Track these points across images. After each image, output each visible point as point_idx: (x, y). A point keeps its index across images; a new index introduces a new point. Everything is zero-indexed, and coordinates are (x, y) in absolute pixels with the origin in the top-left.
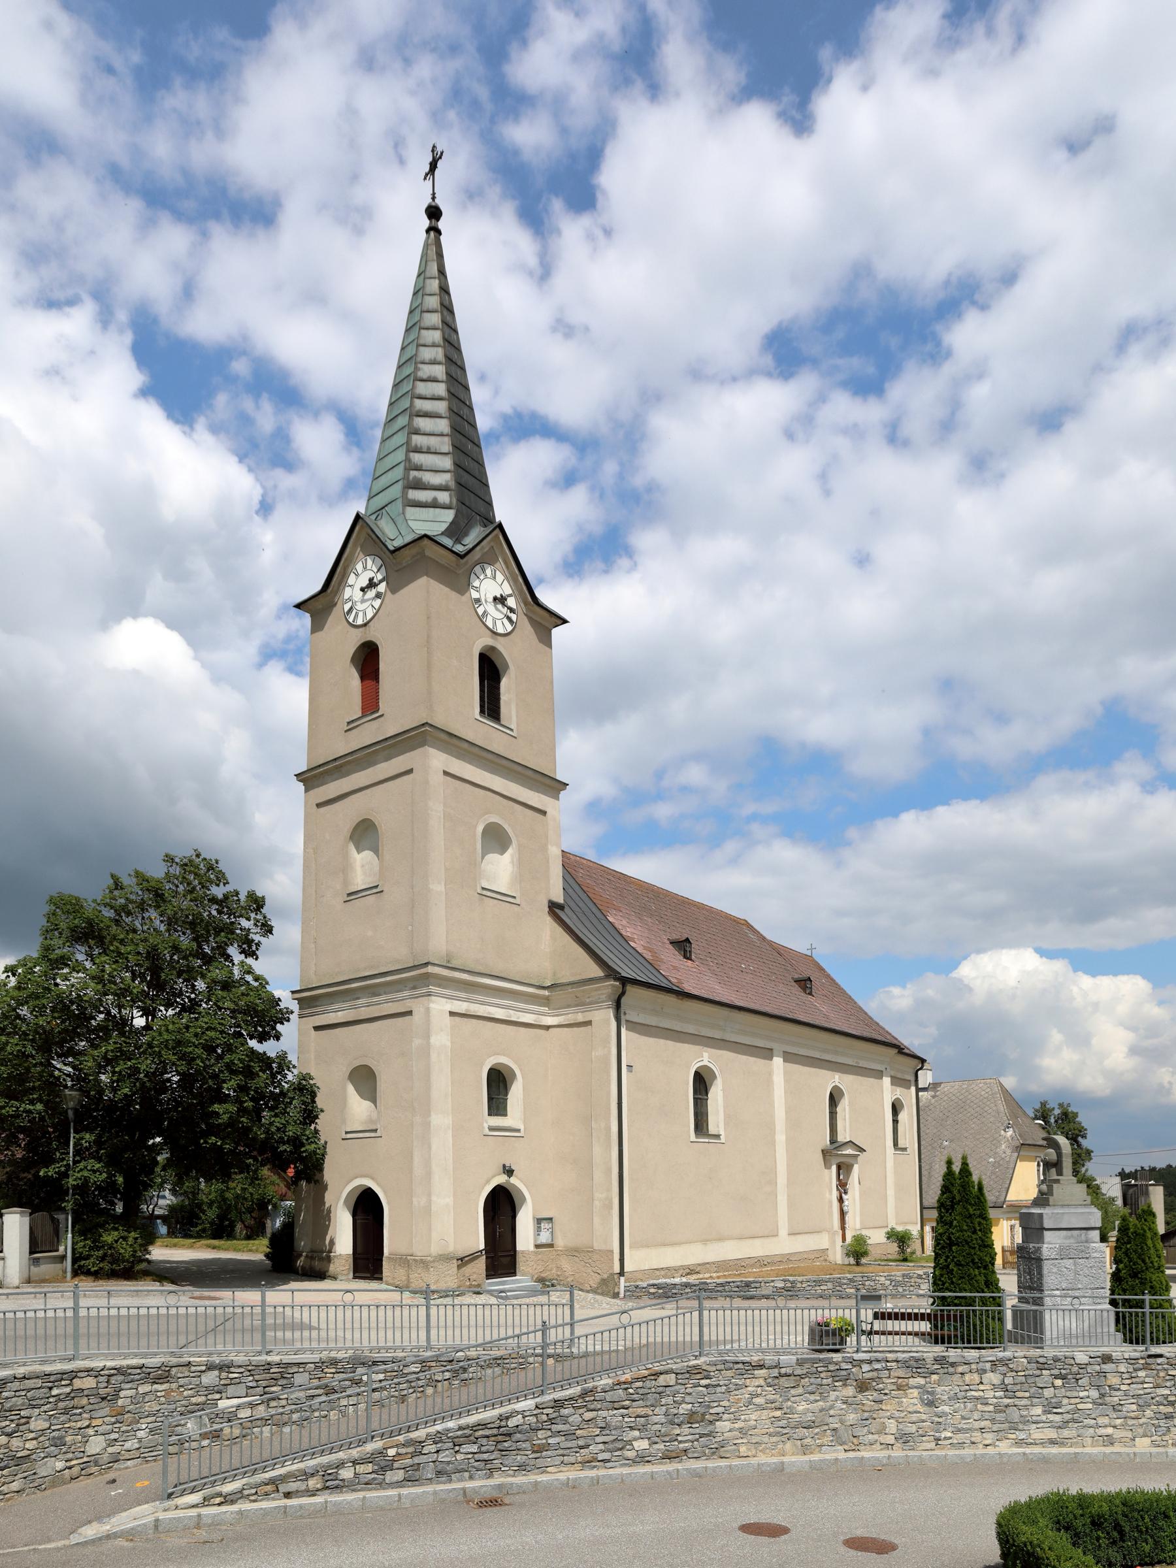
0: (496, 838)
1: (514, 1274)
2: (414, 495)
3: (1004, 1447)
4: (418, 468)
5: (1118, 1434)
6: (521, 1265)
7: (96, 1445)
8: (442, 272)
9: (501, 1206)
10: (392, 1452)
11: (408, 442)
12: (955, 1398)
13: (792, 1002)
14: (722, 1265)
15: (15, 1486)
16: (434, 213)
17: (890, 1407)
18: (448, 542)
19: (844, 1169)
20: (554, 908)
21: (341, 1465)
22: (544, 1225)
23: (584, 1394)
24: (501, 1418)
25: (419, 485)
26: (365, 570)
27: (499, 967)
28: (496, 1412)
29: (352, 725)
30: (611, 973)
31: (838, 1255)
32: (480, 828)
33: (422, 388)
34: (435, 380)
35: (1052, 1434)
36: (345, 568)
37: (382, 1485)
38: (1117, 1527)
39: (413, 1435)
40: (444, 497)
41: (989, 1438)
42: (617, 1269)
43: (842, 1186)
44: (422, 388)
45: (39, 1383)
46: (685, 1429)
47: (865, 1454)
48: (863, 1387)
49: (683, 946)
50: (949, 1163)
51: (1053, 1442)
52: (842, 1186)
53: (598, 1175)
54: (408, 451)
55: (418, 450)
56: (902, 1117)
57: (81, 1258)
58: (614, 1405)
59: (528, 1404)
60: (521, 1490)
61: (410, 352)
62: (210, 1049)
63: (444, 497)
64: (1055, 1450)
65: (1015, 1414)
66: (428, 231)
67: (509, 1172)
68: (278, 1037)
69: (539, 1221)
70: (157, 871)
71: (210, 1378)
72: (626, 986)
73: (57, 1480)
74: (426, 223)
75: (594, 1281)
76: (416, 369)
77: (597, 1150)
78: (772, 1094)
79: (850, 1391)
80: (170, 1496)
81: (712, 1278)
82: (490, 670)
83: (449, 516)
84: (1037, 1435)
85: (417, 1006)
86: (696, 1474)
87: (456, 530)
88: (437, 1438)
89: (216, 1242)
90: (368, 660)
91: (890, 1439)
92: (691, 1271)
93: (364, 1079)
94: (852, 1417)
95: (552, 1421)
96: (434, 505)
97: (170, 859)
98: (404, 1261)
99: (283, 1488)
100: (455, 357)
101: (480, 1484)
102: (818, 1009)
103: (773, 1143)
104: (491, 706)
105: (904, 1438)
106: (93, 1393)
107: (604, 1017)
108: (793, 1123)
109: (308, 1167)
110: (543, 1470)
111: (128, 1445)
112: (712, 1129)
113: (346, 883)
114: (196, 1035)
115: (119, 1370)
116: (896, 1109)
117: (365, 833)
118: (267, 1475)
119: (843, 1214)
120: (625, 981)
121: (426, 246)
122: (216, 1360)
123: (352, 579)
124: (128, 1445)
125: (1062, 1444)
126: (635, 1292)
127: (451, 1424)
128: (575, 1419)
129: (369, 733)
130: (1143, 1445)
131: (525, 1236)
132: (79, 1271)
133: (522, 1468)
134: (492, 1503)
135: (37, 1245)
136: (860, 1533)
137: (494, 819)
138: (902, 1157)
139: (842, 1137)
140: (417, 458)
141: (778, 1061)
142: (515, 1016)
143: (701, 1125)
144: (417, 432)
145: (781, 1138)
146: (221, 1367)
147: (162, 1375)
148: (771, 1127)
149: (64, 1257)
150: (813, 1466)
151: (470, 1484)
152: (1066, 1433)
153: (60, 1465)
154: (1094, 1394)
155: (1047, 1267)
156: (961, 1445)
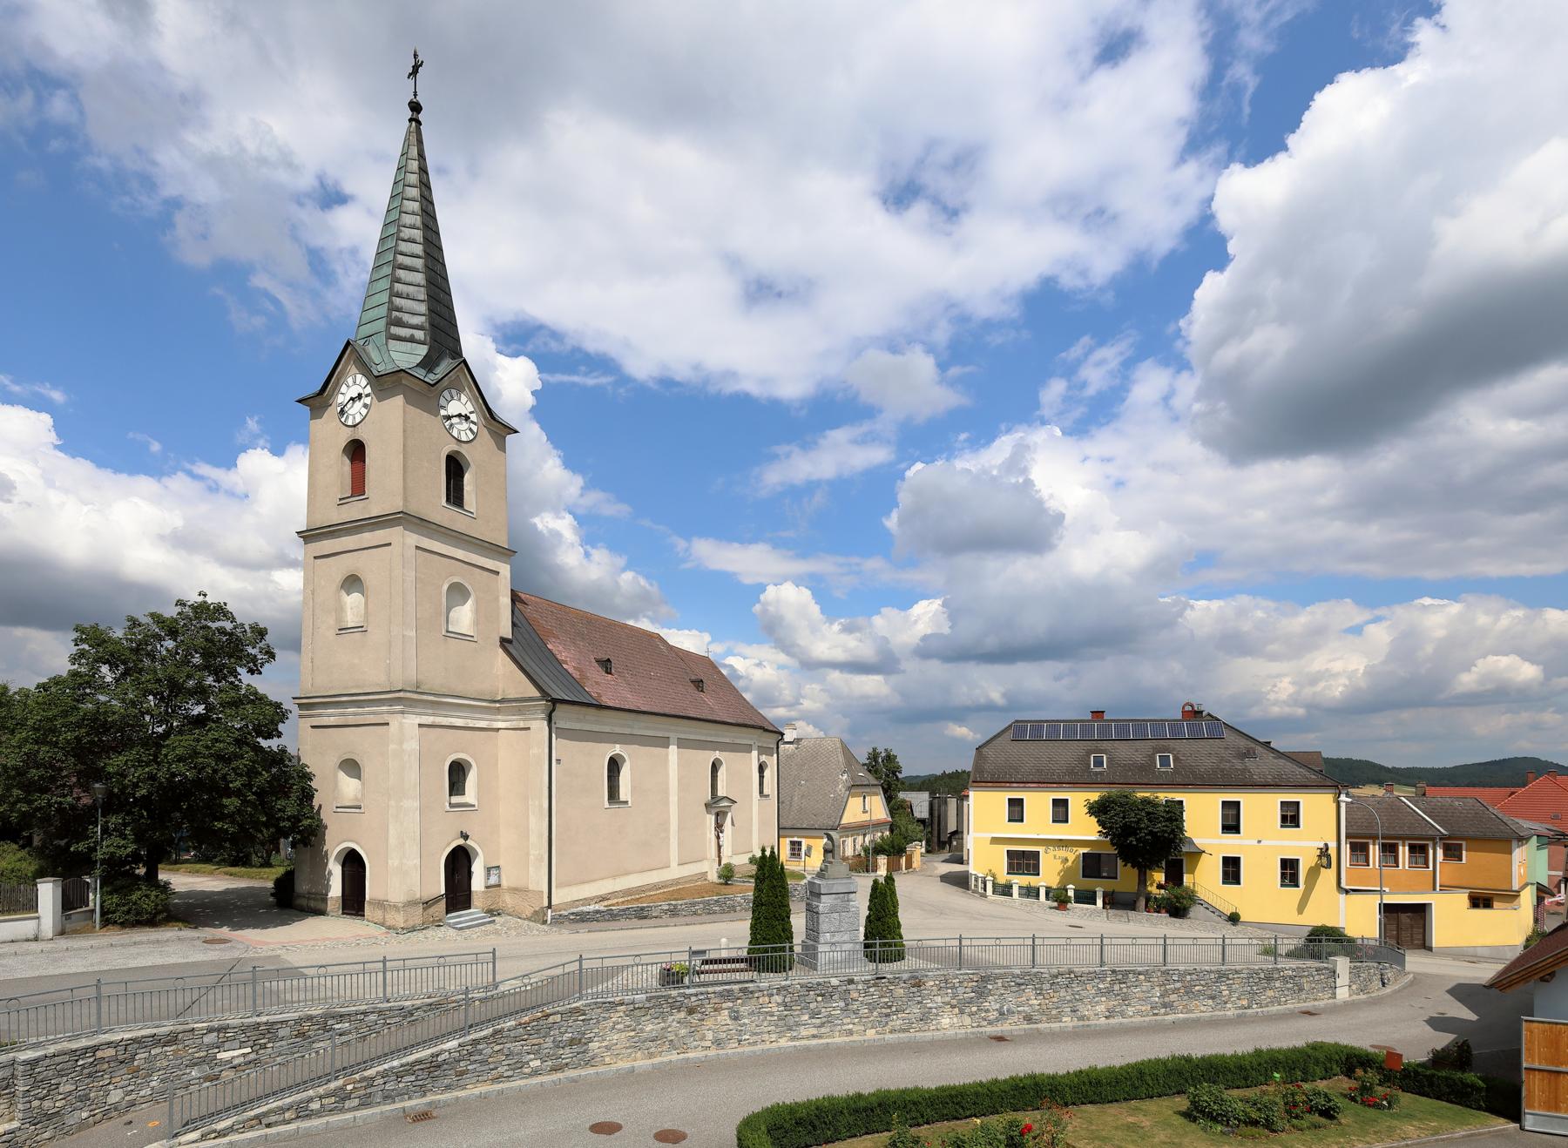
0: (458, 593)
1: (469, 907)
2: (395, 330)
3: (783, 1042)
4: (399, 310)
5: (855, 1028)
6: (476, 901)
7: (115, 1096)
8: (421, 156)
9: (459, 862)
10: (350, 1087)
11: (391, 288)
12: (752, 1013)
13: (687, 701)
14: (628, 892)
15: (46, 1135)
16: (415, 107)
17: (709, 1023)
18: (420, 373)
19: (720, 816)
20: (504, 642)
21: (310, 1100)
22: (493, 872)
23: (495, 1033)
24: (433, 1056)
25: (399, 323)
26: (354, 384)
27: (459, 690)
28: (429, 1052)
29: (343, 501)
30: (545, 694)
31: (713, 876)
32: (445, 587)
33: (403, 247)
34: (414, 242)
35: (814, 1031)
36: (338, 380)
37: (342, 1111)
38: (811, 1123)
39: (366, 1073)
40: (420, 335)
41: (774, 1037)
42: (546, 904)
43: (719, 827)
44: (403, 247)
45: (67, 1058)
46: (567, 1050)
47: (691, 1055)
48: (691, 1011)
49: (606, 665)
50: (763, 850)
51: (814, 1036)
52: (719, 827)
53: (533, 838)
54: (391, 295)
55: (399, 296)
56: (767, 773)
57: (108, 912)
58: (516, 1039)
59: (453, 1044)
60: (446, 1104)
61: (394, 215)
62: (220, 758)
63: (420, 335)
64: (814, 1042)
65: (791, 1021)
66: (411, 120)
67: (466, 837)
68: (279, 735)
69: (489, 870)
70: (171, 612)
71: (210, 1038)
72: (560, 700)
73: (82, 1126)
74: (409, 114)
75: (528, 912)
76: (399, 231)
77: (533, 820)
78: (668, 773)
79: (682, 1015)
80: (176, 1135)
81: (616, 904)
82: (455, 468)
83: (423, 350)
84: (804, 1033)
85: (395, 721)
86: (574, 1080)
87: (428, 363)
88: (384, 1074)
89: (233, 870)
90: (356, 451)
91: (708, 1044)
92: (603, 899)
93: (351, 767)
94: (683, 1032)
95: (470, 1054)
96: (412, 340)
97: (180, 603)
98: (381, 904)
99: (265, 1121)
100: (431, 224)
101: (416, 1103)
102: (709, 703)
103: (667, 803)
104: (455, 495)
105: (718, 1043)
106: (115, 1059)
107: (539, 726)
108: (683, 786)
109: (309, 834)
110: (464, 1087)
111: (142, 1093)
112: (622, 797)
113: (339, 619)
114: (207, 747)
115: (134, 1040)
116: (761, 768)
117: (352, 582)
118: (252, 1113)
119: (719, 847)
120: (555, 702)
121: (409, 132)
122: (215, 1024)
123: (344, 389)
124: (142, 1093)
125: (820, 1037)
126: (559, 920)
127: (395, 1063)
128: (488, 1051)
129: (355, 511)
130: (871, 1033)
131: (478, 883)
132: (107, 921)
133: (448, 1088)
134: (423, 1116)
135: (70, 902)
136: (667, 1126)
137: (456, 580)
138: (765, 801)
139: (720, 794)
140: (398, 301)
141: (673, 749)
142: (471, 723)
143: (613, 794)
144: (399, 281)
145: (674, 799)
146: (219, 1030)
147: (172, 1039)
148: (666, 792)
149: (93, 911)
150: (656, 1068)
151: (408, 1104)
152: (823, 1030)
153: (85, 1115)
154: (842, 1004)
155: (822, 918)
156: (755, 1043)
